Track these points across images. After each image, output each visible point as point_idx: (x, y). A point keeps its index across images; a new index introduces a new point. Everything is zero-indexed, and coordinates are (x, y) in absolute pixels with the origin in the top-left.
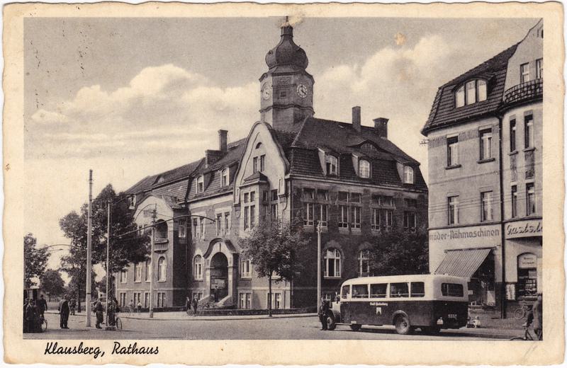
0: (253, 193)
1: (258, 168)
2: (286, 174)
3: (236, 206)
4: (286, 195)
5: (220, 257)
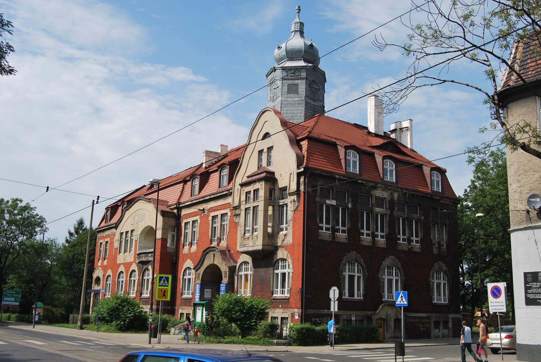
0: (256, 191)
1: (264, 163)
2: (298, 167)
3: (235, 208)
4: (297, 192)
5: (214, 271)
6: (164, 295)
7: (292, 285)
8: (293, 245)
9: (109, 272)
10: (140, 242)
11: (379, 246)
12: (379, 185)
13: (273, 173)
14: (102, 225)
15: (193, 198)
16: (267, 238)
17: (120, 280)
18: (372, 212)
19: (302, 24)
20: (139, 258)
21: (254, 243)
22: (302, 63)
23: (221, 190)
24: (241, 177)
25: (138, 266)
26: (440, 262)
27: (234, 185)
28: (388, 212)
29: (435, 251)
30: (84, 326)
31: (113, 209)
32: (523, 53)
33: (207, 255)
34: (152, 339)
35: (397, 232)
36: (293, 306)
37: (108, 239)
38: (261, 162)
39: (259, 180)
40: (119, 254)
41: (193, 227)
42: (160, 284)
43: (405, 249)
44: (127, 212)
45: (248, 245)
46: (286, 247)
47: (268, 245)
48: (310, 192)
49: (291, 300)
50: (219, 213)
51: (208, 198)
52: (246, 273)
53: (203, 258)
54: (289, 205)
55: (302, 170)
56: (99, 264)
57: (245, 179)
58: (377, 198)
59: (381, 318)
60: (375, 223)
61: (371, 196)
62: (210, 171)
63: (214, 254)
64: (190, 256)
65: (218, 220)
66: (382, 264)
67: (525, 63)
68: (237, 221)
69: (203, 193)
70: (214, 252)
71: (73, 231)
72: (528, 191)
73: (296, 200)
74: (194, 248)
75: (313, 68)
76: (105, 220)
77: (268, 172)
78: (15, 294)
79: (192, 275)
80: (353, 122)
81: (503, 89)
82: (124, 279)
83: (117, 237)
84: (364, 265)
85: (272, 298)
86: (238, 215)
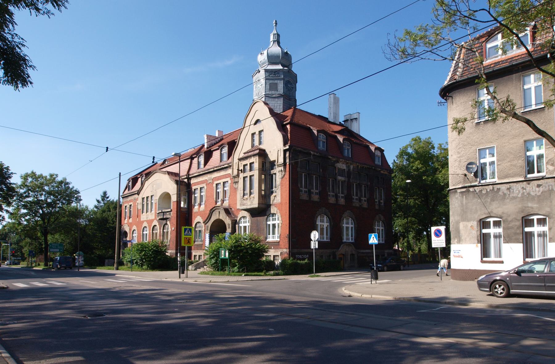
0: (251, 164)
1: (256, 143)
3: (234, 177)
6: (189, 242)
7: (281, 232)
8: (281, 203)
9: (134, 227)
10: (159, 204)
11: (340, 204)
12: (341, 160)
13: (264, 151)
14: (126, 193)
15: (199, 170)
16: (261, 198)
17: (145, 233)
18: (336, 179)
19: (278, 35)
20: (158, 216)
21: (252, 203)
22: (280, 67)
23: (222, 164)
24: (239, 153)
25: (158, 222)
26: (380, 215)
27: (233, 160)
28: (347, 180)
29: (377, 207)
30: (120, 268)
31: (134, 180)
32: (466, 54)
33: (214, 212)
34: (182, 275)
35: (352, 194)
36: (282, 247)
37: (131, 203)
38: (254, 142)
39: (254, 155)
40: (142, 213)
41: (224, 186)
42: (185, 234)
43: (358, 205)
44: (147, 182)
45: (246, 204)
46: (276, 205)
47: (263, 204)
48: (293, 164)
49: (280, 243)
50: (221, 181)
51: (212, 170)
52: (274, 222)
53: (210, 215)
54: (278, 174)
55: (287, 147)
56: (126, 221)
57: (242, 155)
58: (339, 169)
59: (342, 254)
60: (337, 187)
61: (335, 167)
62: (212, 150)
63: (219, 212)
64: (200, 213)
65: (220, 186)
66: (342, 216)
67: (468, 62)
68: (236, 187)
69: (207, 167)
70: (219, 210)
71: (100, 199)
72: (465, 160)
73: (283, 170)
74: (203, 207)
75: (289, 71)
76: (127, 189)
77: (261, 150)
78: (59, 246)
79: (202, 227)
80: (317, 114)
81: (450, 83)
82: (147, 232)
83: (140, 201)
84: (330, 217)
85: (266, 242)
86: (237, 182)
